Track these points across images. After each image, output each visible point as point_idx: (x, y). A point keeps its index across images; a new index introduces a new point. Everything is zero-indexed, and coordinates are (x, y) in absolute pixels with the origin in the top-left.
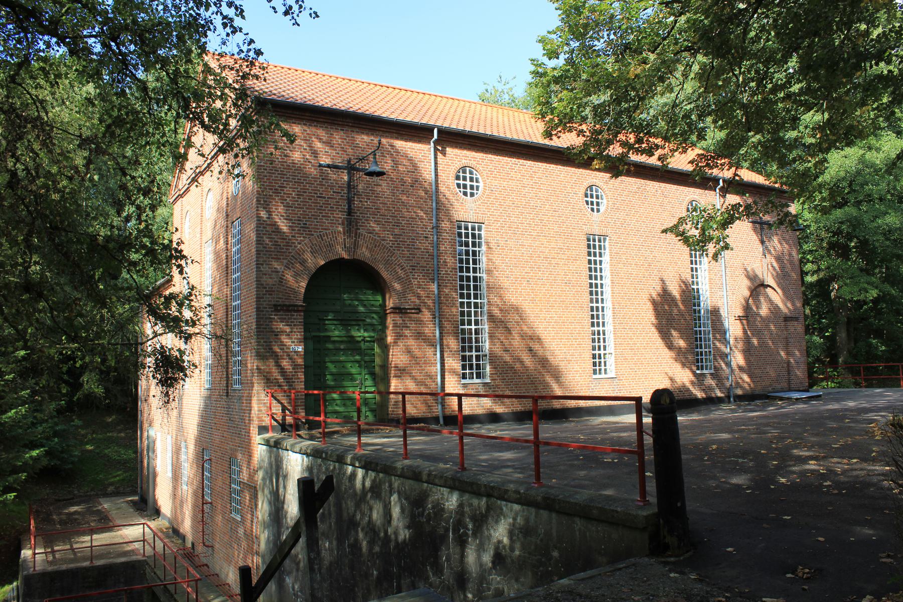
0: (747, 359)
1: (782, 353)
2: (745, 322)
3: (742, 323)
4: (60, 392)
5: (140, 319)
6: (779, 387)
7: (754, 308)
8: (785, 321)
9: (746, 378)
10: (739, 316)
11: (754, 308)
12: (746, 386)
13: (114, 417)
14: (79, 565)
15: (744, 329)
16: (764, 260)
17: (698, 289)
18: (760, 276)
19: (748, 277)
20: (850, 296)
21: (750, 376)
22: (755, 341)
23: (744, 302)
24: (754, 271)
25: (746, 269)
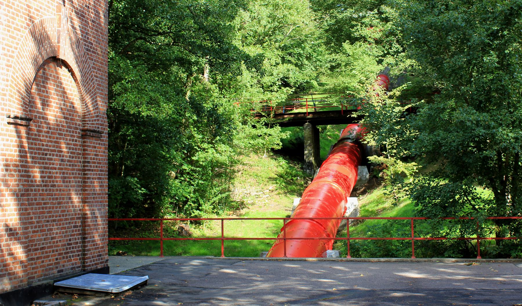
0: (23, 213)
1: (76, 199)
2: (23, 130)
3: (18, 132)
4: (472, 141)
5: (410, 25)
6: (67, 266)
7: (39, 106)
8: (83, 136)
9: (19, 251)
10: (16, 117)
11: (39, 106)
12: (18, 269)
13: (447, 182)
14: (488, 279)
15: (21, 146)
16: (63, 9)
17: (59, 46)
18: (54, 40)
19: (33, 34)
20: (136, 109)
21: (28, 250)
22: (37, 174)
23: (23, 90)
24: (42, 23)
25: (31, 20)
